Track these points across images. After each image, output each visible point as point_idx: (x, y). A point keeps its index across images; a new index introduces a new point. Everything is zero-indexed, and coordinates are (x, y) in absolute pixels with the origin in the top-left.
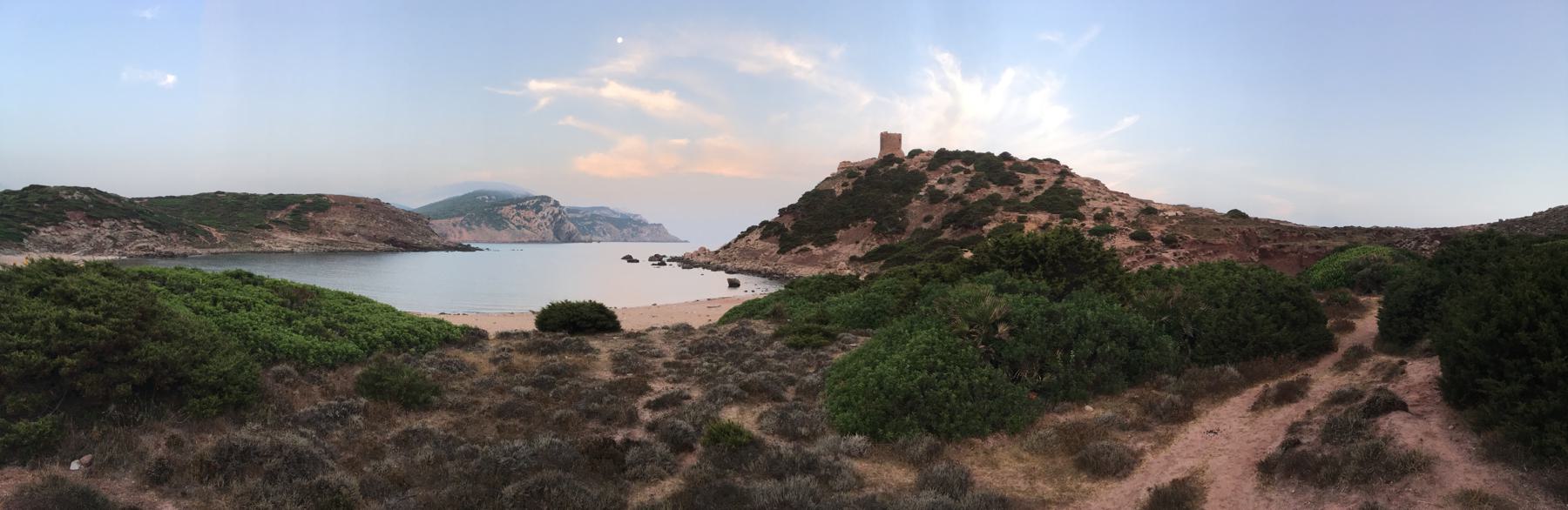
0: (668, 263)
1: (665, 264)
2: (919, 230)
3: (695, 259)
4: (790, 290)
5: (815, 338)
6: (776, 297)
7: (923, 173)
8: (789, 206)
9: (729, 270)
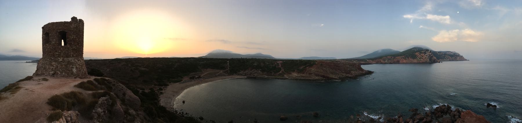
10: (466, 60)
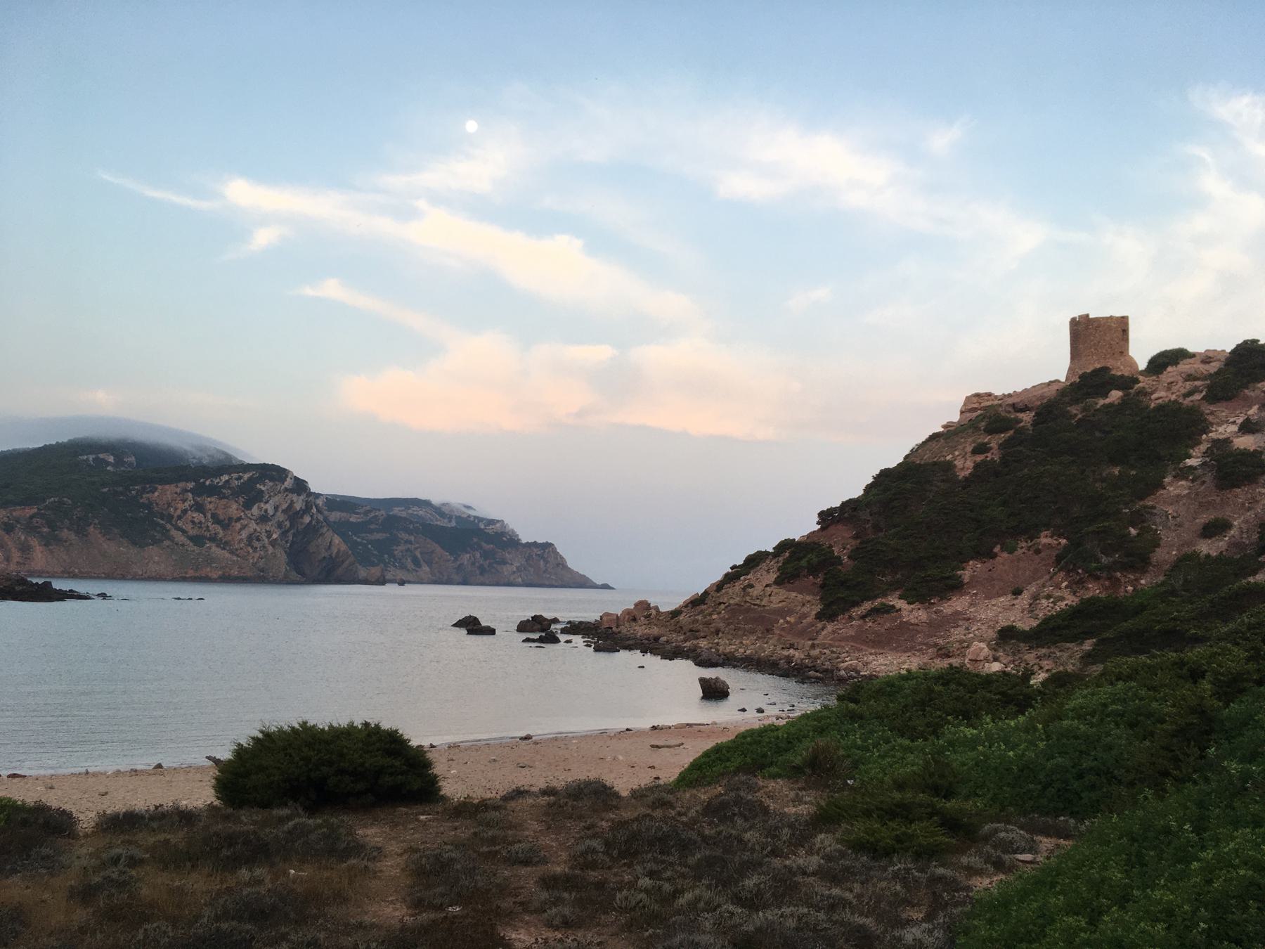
0: (563, 638)
1: (556, 641)
2: (1188, 560)
3: (624, 630)
4: (852, 706)
5: (919, 830)
6: (815, 723)
7: (1193, 412)
8: (844, 504)
9: (704, 656)
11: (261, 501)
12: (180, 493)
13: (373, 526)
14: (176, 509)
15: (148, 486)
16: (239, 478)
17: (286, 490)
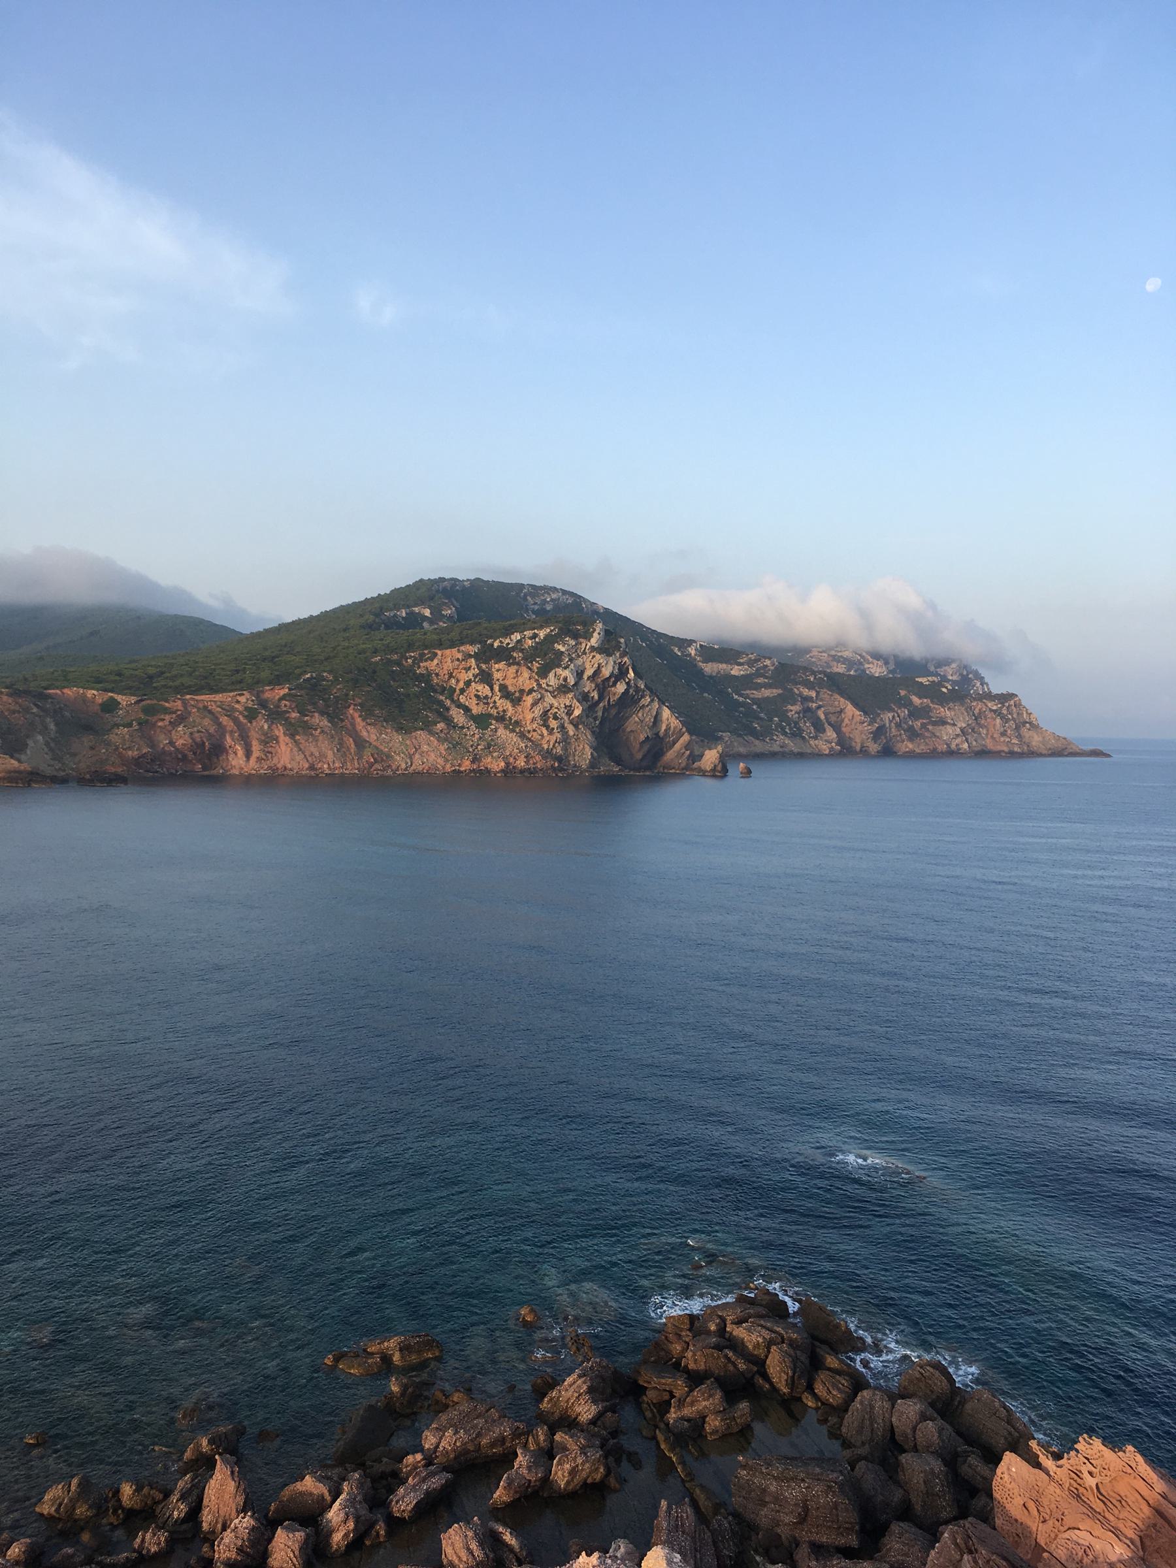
10: (1062, 751)
11: (559, 666)
12: (463, 660)
13: (760, 680)
14: (458, 681)
15: (426, 652)
16: (535, 636)
17: (593, 649)
